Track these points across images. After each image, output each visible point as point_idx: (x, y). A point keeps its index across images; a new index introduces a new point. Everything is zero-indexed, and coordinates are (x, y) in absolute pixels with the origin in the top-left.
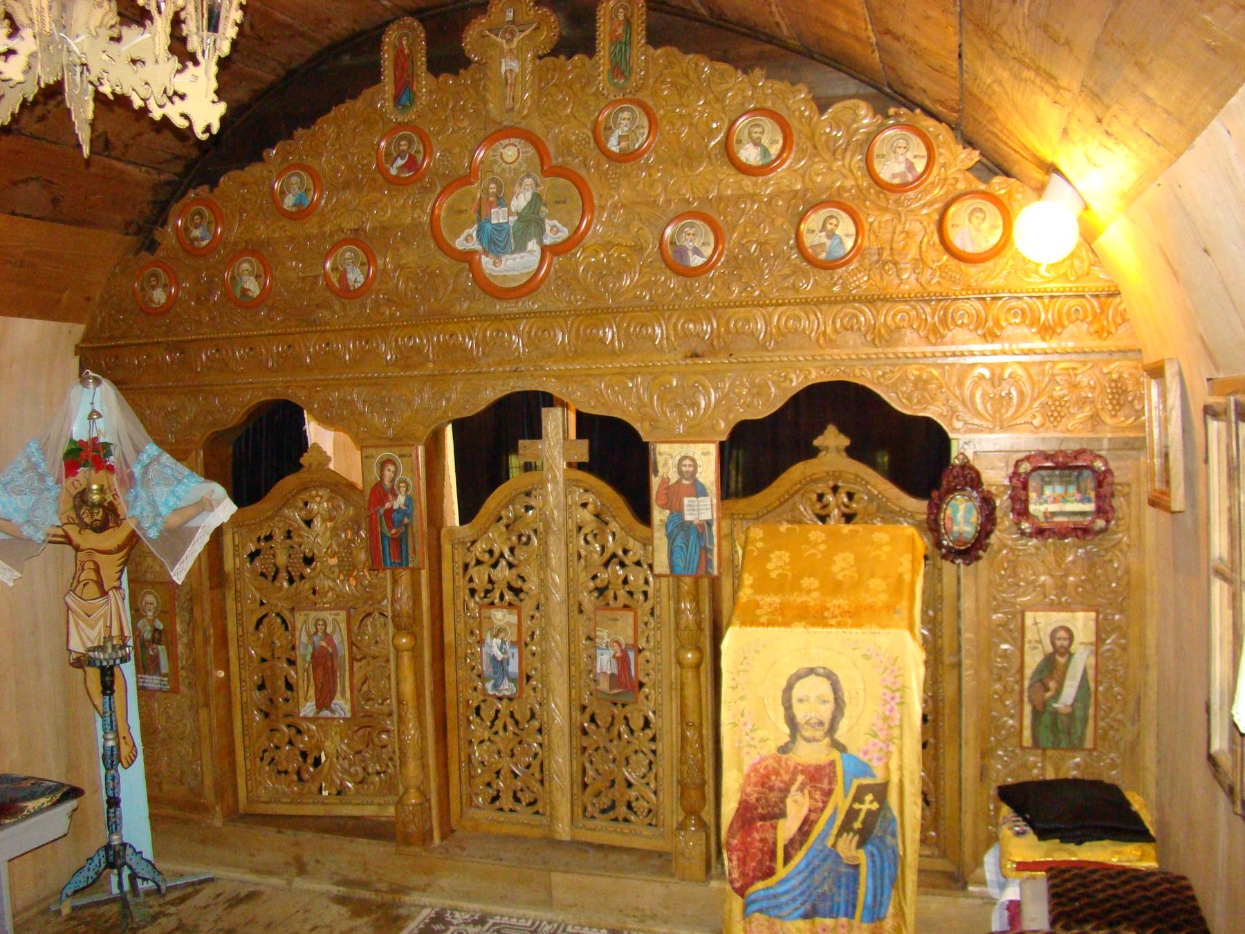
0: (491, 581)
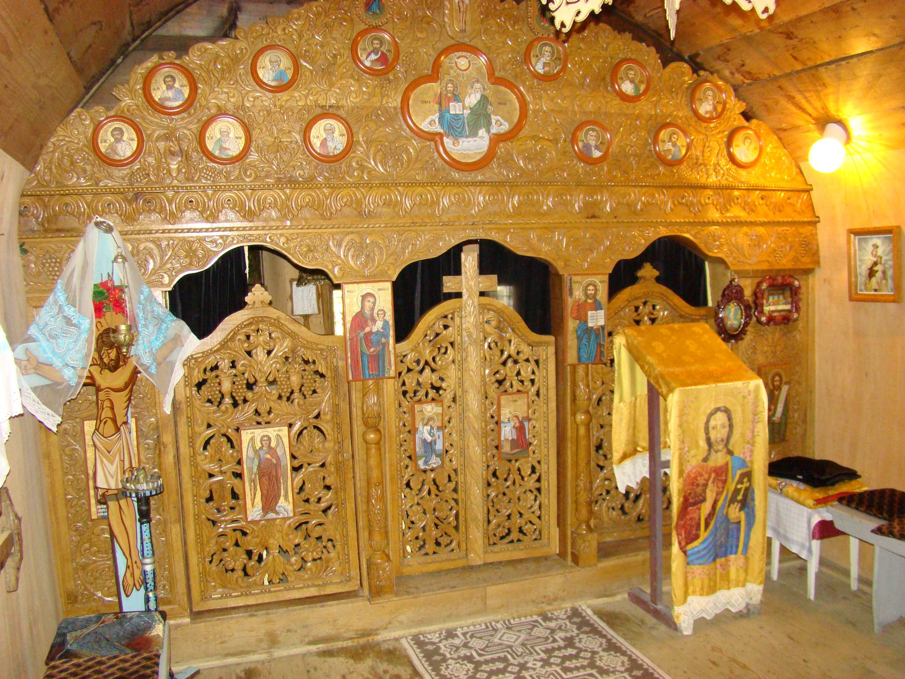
0: (419, 384)
